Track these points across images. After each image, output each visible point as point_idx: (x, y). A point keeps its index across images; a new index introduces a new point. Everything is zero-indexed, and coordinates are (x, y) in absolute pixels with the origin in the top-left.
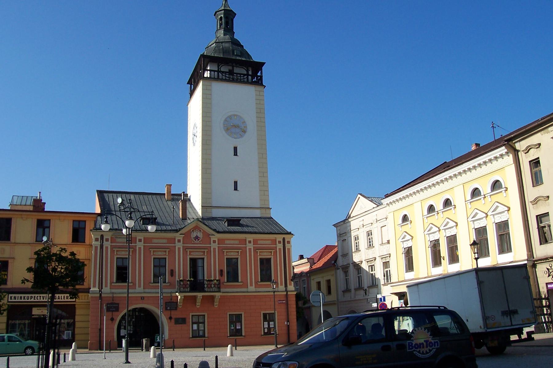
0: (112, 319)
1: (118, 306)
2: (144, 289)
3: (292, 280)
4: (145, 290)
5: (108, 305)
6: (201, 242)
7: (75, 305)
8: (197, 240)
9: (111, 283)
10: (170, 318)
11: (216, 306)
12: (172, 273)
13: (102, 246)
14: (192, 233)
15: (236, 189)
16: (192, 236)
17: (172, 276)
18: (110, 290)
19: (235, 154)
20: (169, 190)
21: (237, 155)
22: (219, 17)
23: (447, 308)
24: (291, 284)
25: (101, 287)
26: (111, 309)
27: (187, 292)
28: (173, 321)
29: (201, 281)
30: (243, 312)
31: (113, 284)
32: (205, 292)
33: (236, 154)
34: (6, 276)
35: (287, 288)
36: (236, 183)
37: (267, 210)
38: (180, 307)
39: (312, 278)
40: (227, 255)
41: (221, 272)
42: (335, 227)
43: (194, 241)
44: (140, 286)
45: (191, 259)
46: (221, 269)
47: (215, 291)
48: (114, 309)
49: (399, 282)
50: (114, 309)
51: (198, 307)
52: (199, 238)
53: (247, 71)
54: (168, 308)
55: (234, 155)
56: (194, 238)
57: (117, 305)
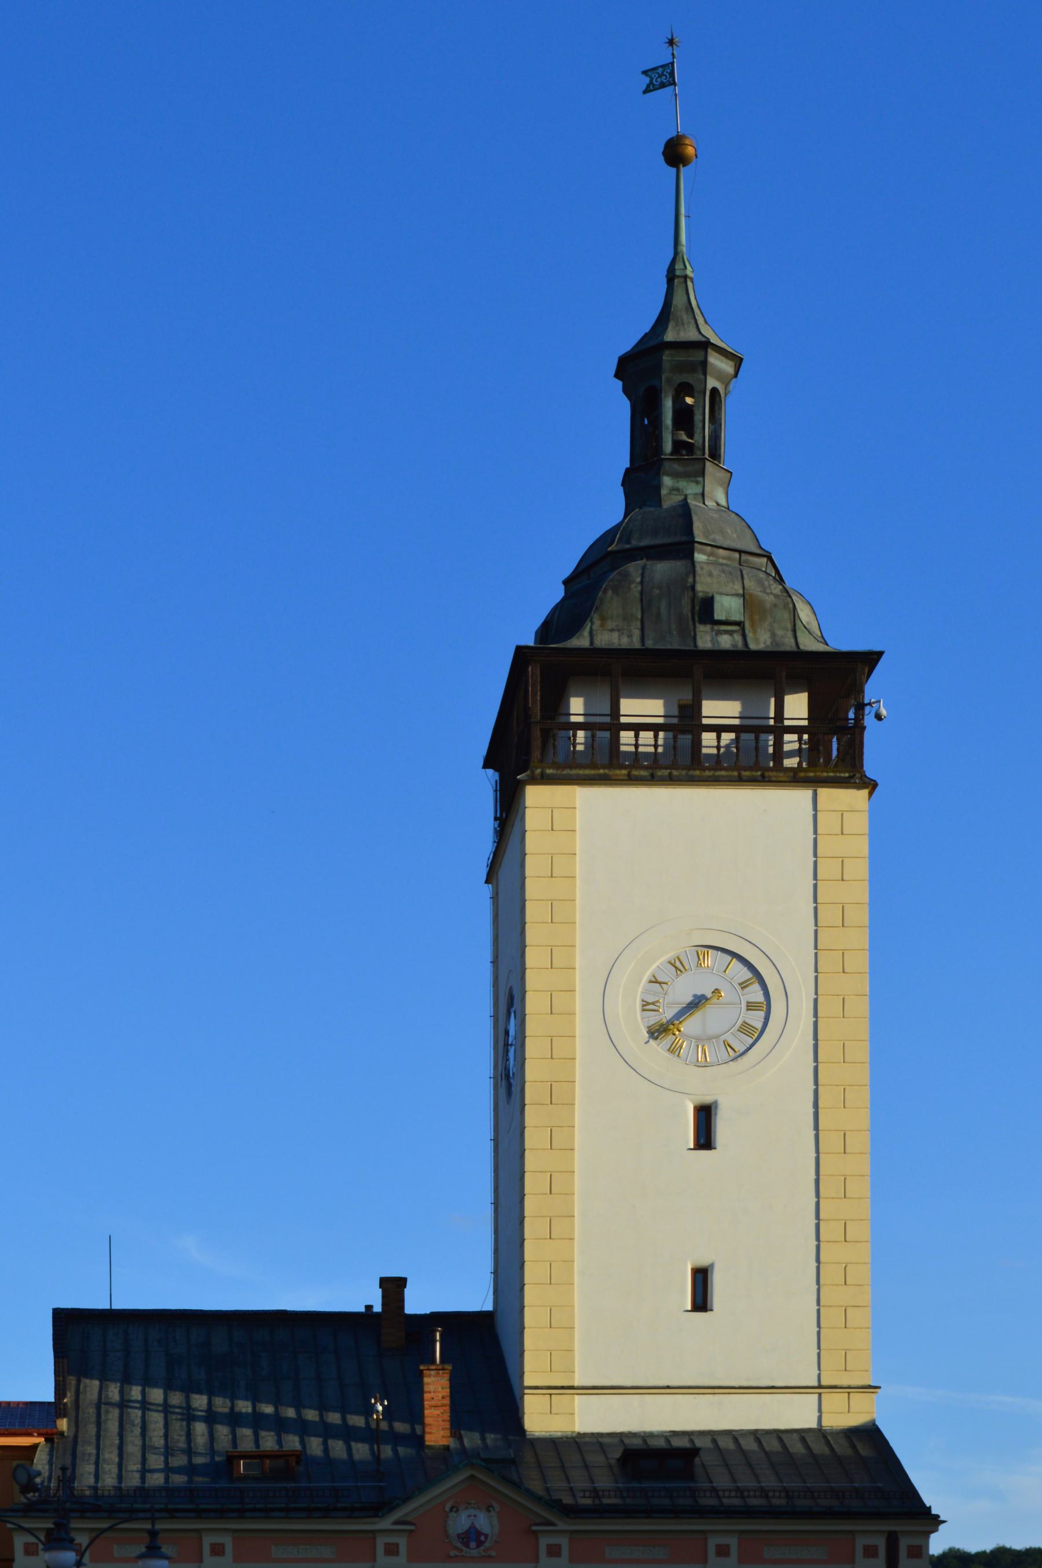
6: (493, 1554)
8: (473, 1544)
19: (702, 1141)
23: (786, 582)
33: (701, 1302)
52: (482, 1538)
56: (458, 1535)
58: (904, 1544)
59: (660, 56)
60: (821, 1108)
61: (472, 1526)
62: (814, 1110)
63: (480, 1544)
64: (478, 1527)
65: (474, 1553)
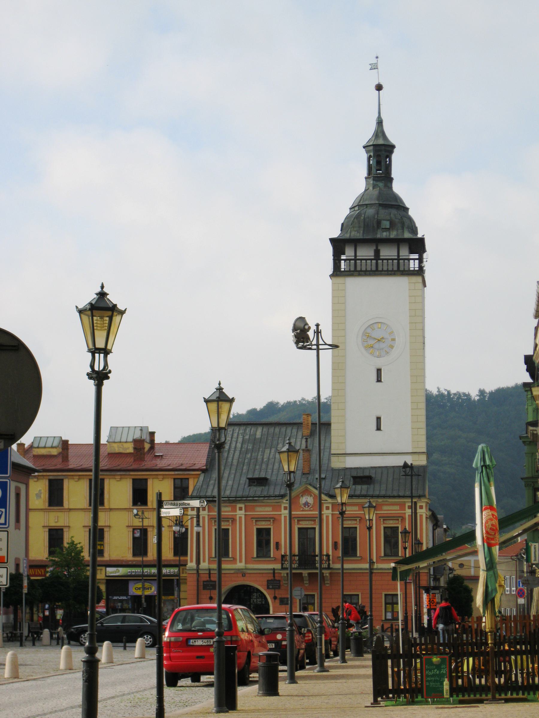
2: (246, 563)
5: (205, 583)
6: (312, 509)
8: (307, 506)
10: (275, 598)
11: (327, 585)
13: (198, 516)
14: (301, 498)
17: (277, 550)
18: (209, 566)
19: (379, 371)
25: (198, 562)
26: (208, 588)
28: (278, 601)
31: (211, 559)
34: (102, 546)
36: (379, 419)
40: (384, 523)
41: (335, 545)
45: (258, 529)
48: (211, 587)
49: (28, 510)
51: (307, 585)
57: (214, 583)
58: (418, 505)
59: (375, 61)
60: (253, 476)
61: (307, 501)
62: (474, 395)
63: (308, 506)
64: (308, 502)
65: (307, 509)
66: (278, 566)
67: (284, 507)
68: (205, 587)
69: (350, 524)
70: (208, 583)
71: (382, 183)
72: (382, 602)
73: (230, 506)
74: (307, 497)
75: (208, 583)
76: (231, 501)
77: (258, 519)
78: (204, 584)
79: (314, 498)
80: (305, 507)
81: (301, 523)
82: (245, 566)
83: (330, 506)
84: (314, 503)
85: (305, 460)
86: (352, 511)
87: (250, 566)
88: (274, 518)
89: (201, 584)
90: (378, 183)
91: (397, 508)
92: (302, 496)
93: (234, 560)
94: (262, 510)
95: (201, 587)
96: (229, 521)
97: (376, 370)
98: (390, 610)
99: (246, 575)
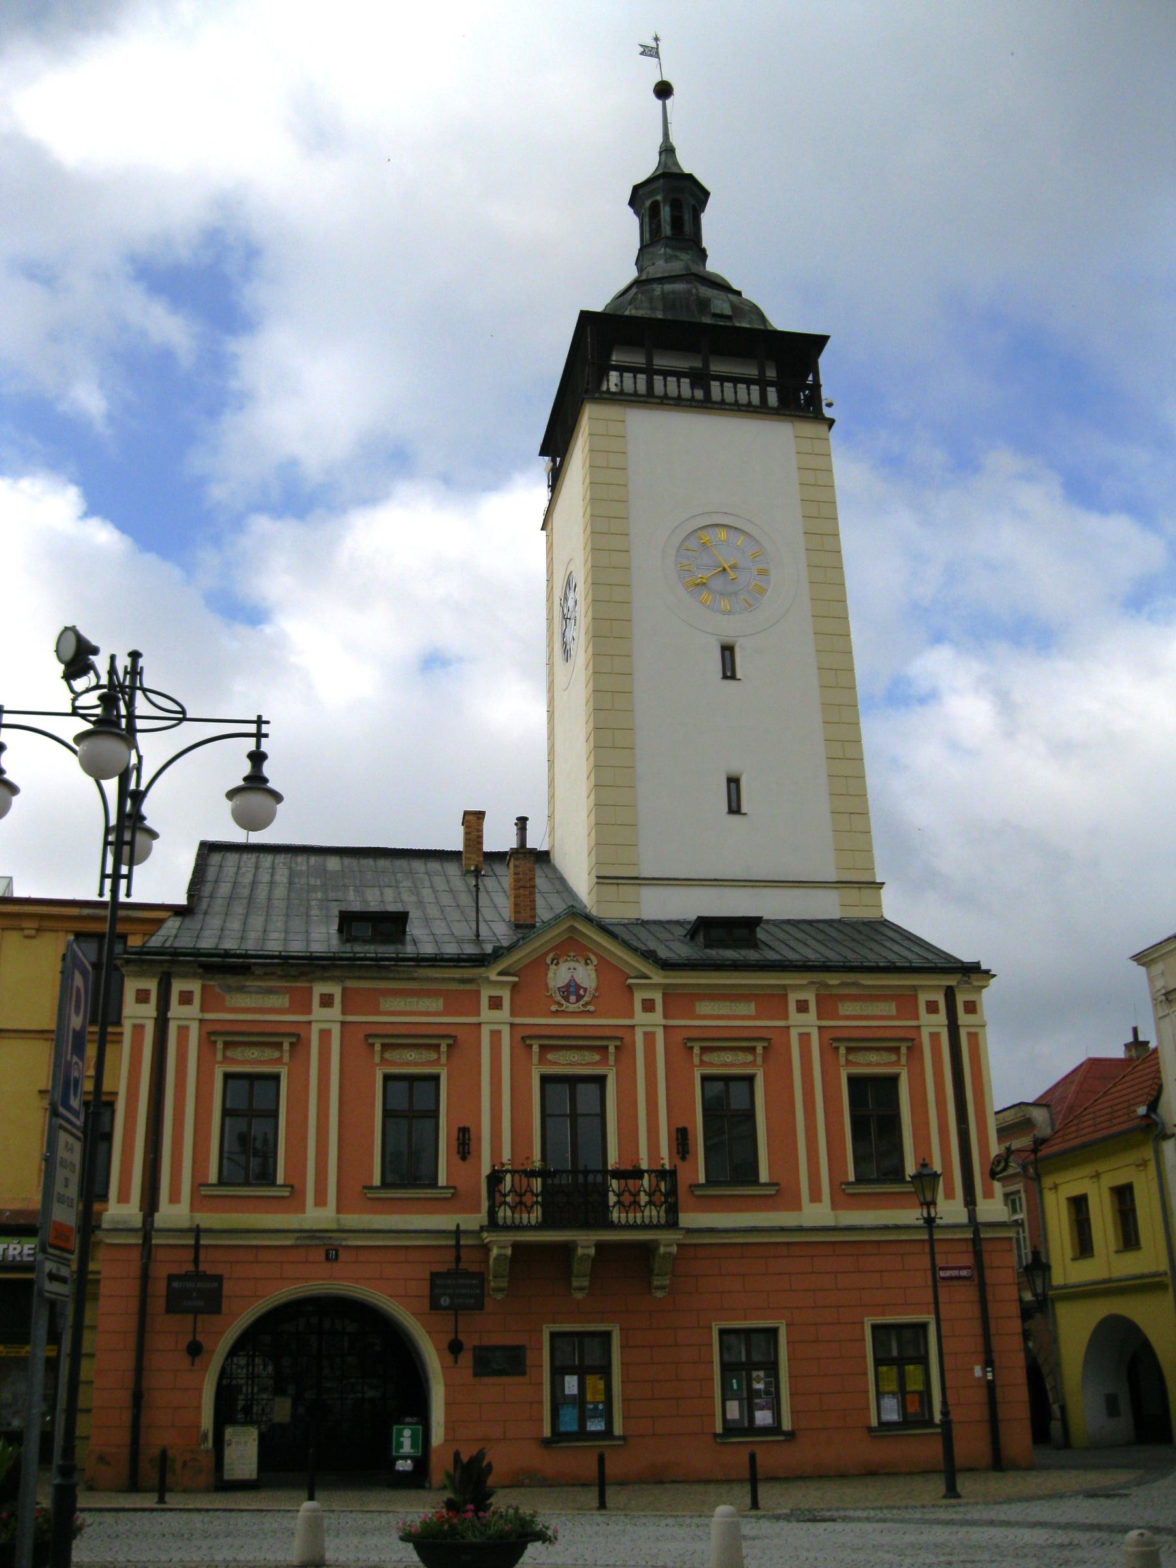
0: (195, 1350)
1: (220, 1288)
2: (339, 1210)
3: (993, 1175)
4: (341, 1216)
5: (175, 1284)
6: (591, 1008)
7: (30, 1283)
8: (573, 998)
9: (199, 1184)
10: (455, 1348)
12: (465, 1143)
13: (162, 1023)
14: (553, 967)
15: (735, 808)
16: (552, 984)
17: (464, 1158)
18: (192, 1218)
19: (729, 674)
20: (475, 834)
21: (733, 677)
22: (648, 203)
24: (989, 1194)
27: (529, 1227)
28: (466, 1359)
29: (591, 1178)
30: (784, 1321)
31: (204, 1191)
32: (612, 1226)
33: (729, 672)
35: (974, 1210)
36: (733, 782)
37: (867, 893)
38: (499, 1296)
39: (1047, 1182)
40: (849, 1063)
41: (681, 1139)
42: (1143, 965)
43: (560, 1005)
44: (320, 1201)
46: (680, 1126)
47: (655, 1221)
48: (201, 1303)
50: (201, 1303)
51: (579, 1296)
52: (582, 992)
53: (762, 371)
54: (445, 1301)
55: (725, 677)
58: (960, 999)
61: (572, 980)
63: (579, 998)
64: (579, 981)
65: (572, 1007)
66: (473, 1220)
67: (491, 998)
68: (176, 1303)
69: (733, 1065)
70: (189, 1285)
71: (688, 254)
72: (865, 1357)
73: (287, 990)
74: (572, 964)
75: (189, 1285)
76: (293, 971)
77: (394, 1041)
78: (170, 1290)
79: (597, 969)
80: (567, 999)
81: (550, 1056)
82: (338, 1221)
83: (658, 997)
84: (596, 990)
85: (521, 883)
86: (729, 1017)
87: (353, 1220)
88: (454, 1038)
89: (159, 1288)
90: (678, 253)
91: (890, 1008)
92: (556, 961)
93: (294, 1198)
94: (408, 1008)
95: (158, 1303)
96: (281, 1044)
97: (719, 649)
98: (893, 1387)
99: (343, 1256)
